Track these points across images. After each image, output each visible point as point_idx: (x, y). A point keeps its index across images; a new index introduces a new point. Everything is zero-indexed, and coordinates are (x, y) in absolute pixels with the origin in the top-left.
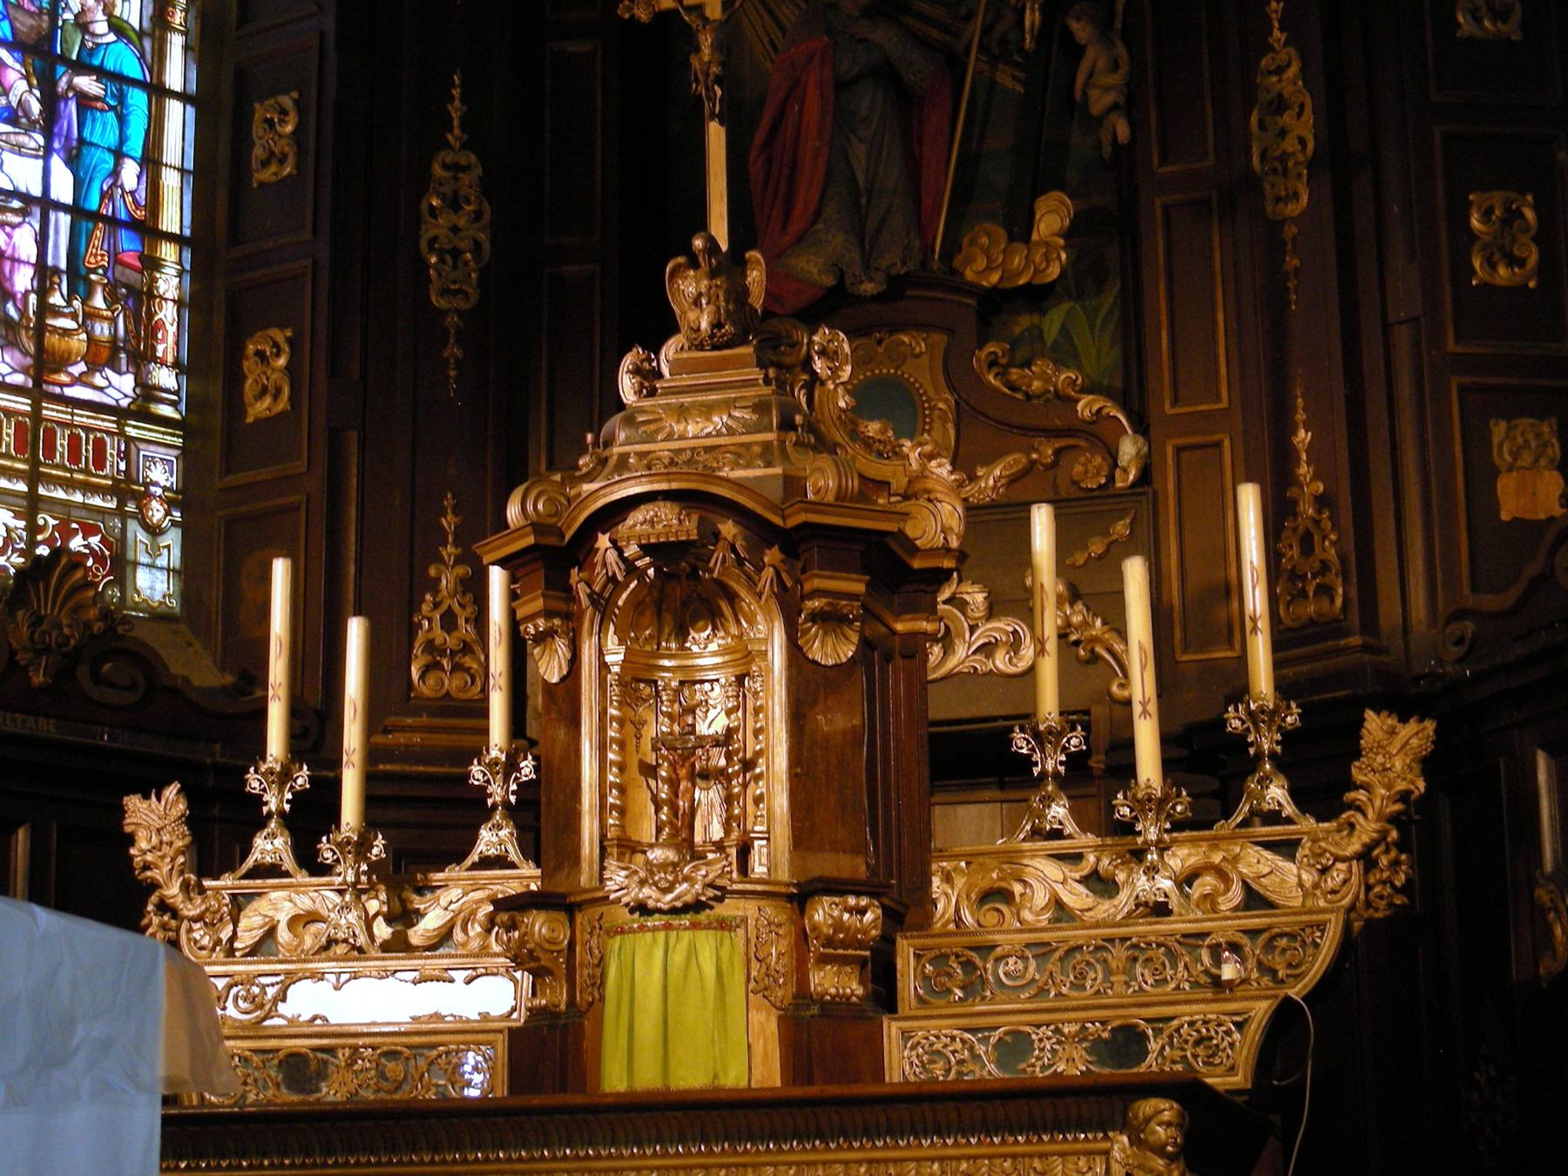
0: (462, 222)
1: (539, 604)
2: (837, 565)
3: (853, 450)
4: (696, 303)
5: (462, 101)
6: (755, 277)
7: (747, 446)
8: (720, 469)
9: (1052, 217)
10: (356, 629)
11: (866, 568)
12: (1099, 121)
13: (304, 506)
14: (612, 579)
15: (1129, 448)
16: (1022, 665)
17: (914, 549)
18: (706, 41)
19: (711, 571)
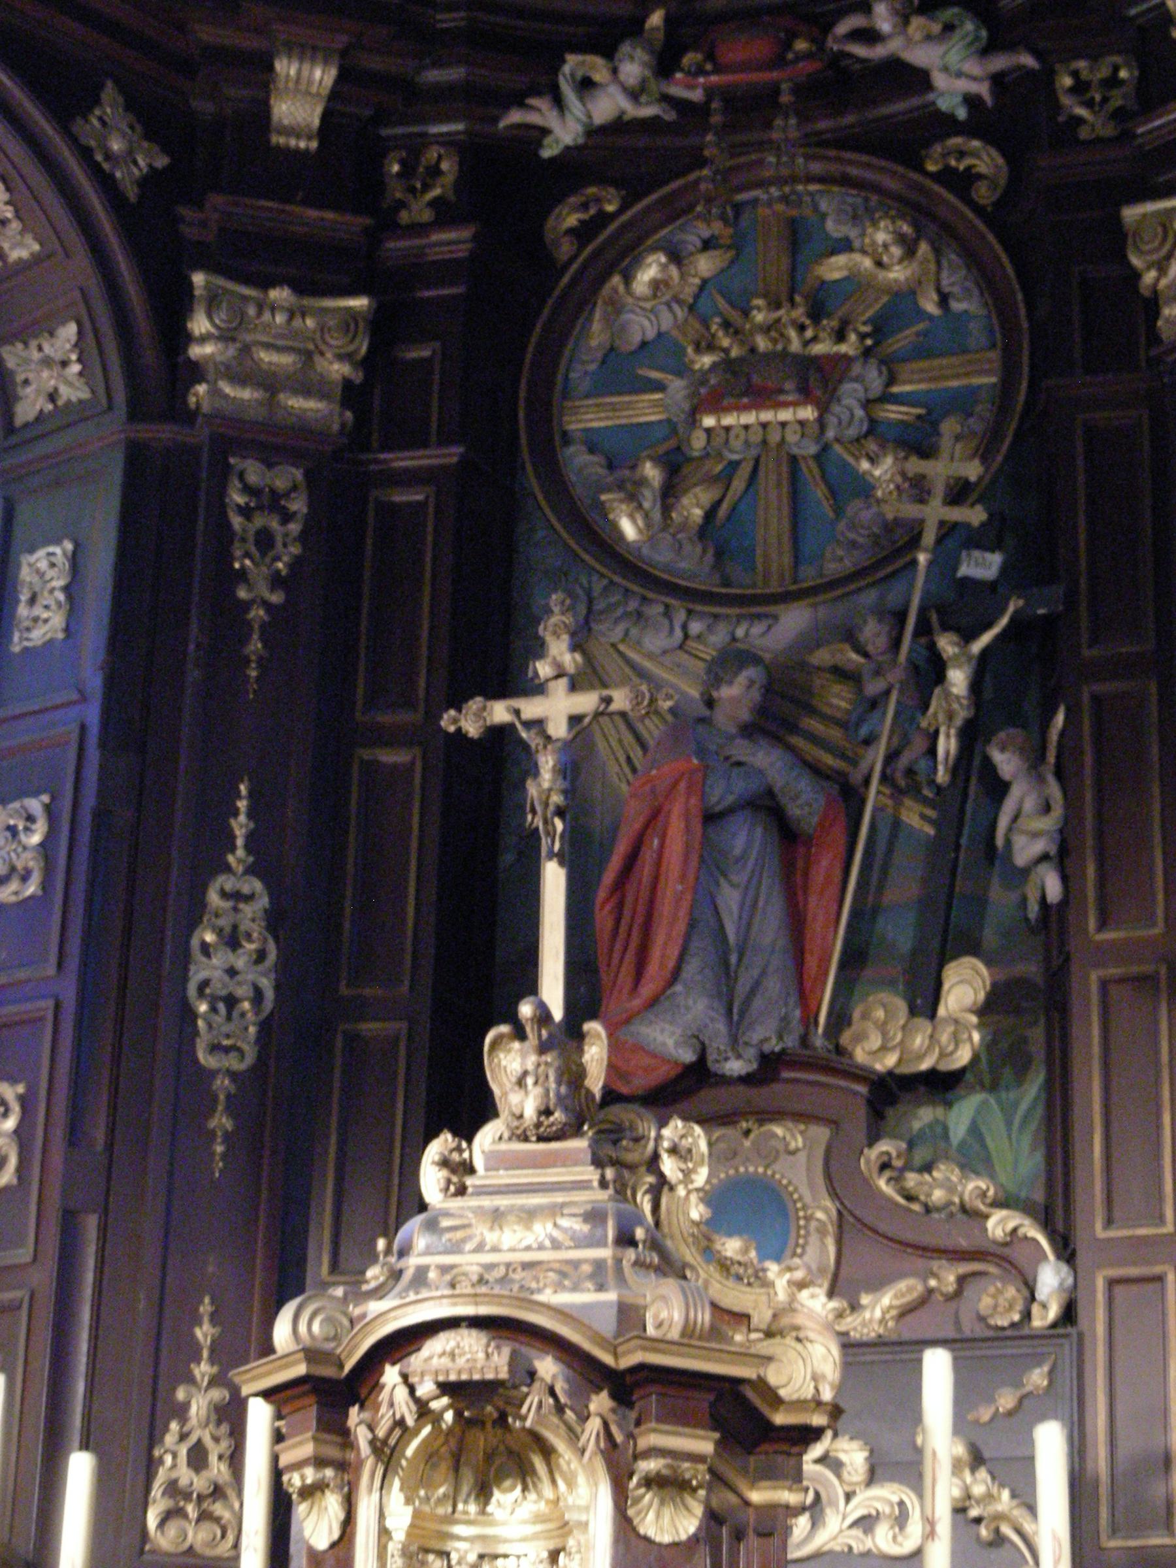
0: (240, 963)
1: (307, 1449)
2: (682, 1419)
3: (704, 1273)
4: (521, 1082)
5: (250, 816)
6: (595, 1054)
7: (576, 1264)
8: (539, 1291)
9: (964, 987)
10: (80, 1469)
11: (716, 1422)
12: (1025, 873)
13: (25, 1306)
14: (400, 1423)
15: (1051, 1279)
16: (908, 1546)
17: (776, 1401)
18: (547, 763)
19: (524, 1419)
